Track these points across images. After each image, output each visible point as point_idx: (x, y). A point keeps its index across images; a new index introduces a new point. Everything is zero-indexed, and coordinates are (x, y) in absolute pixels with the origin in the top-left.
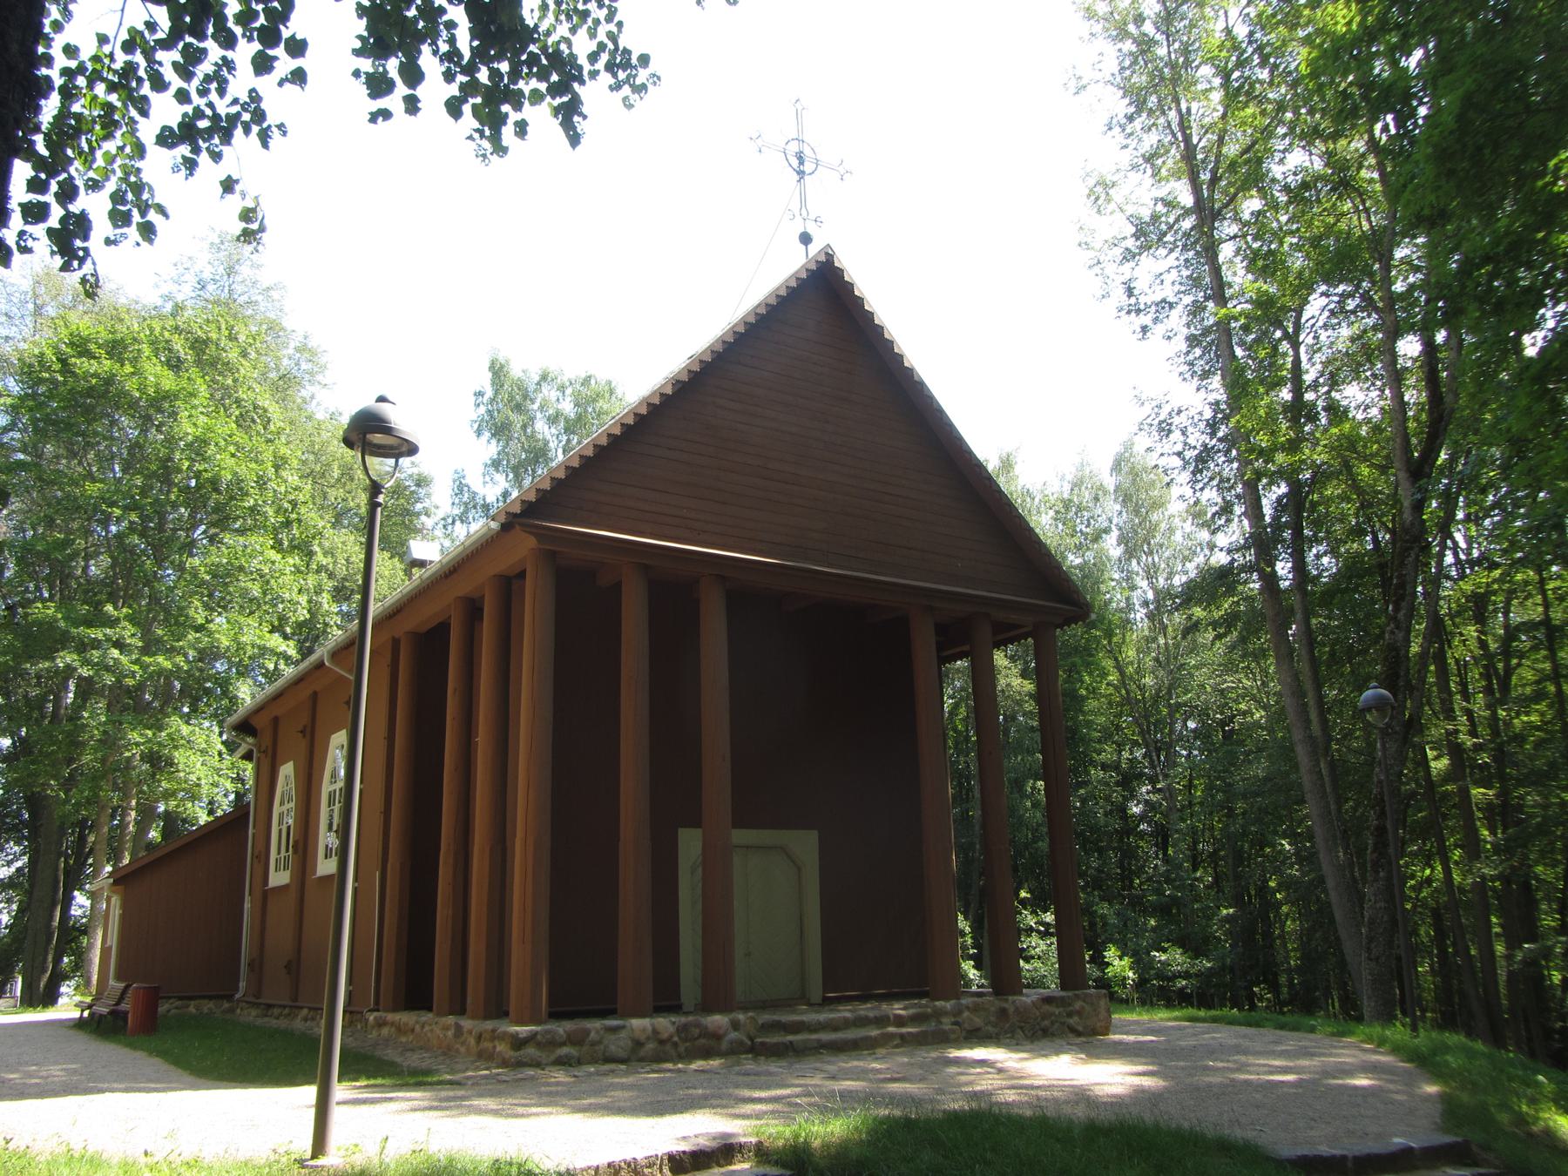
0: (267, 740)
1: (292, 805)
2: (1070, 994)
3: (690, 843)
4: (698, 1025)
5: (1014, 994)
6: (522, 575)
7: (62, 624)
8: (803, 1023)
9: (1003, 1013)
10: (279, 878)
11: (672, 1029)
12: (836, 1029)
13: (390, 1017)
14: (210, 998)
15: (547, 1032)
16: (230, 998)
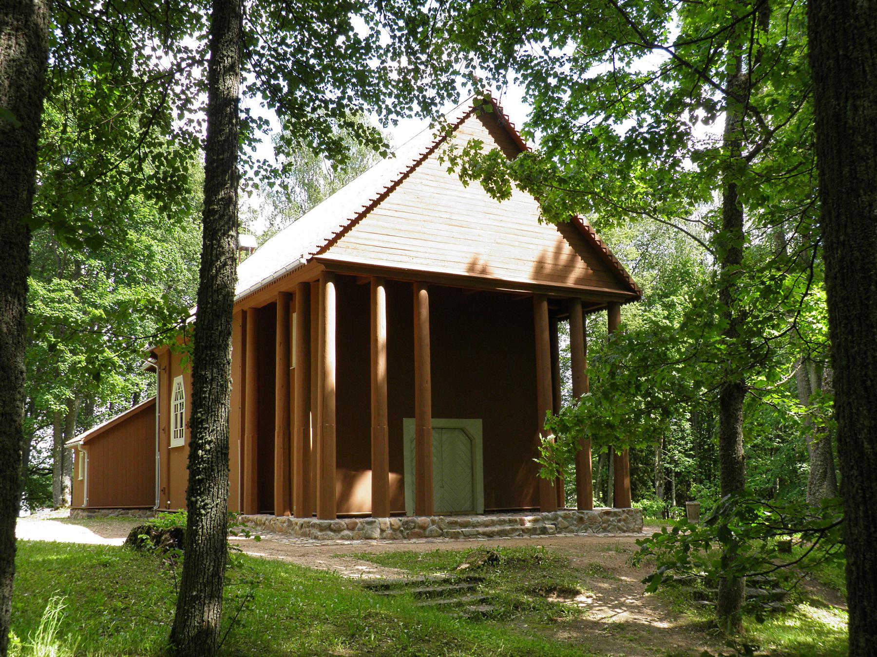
0: (165, 363)
1: (184, 400)
2: (620, 510)
3: (409, 426)
4: (413, 522)
5: (587, 509)
6: (318, 280)
7: (623, 599)
8: (469, 522)
9: (581, 519)
10: (177, 442)
11: (400, 523)
12: (487, 526)
13: (251, 517)
14: (140, 509)
15: (336, 523)
16: (150, 509)
